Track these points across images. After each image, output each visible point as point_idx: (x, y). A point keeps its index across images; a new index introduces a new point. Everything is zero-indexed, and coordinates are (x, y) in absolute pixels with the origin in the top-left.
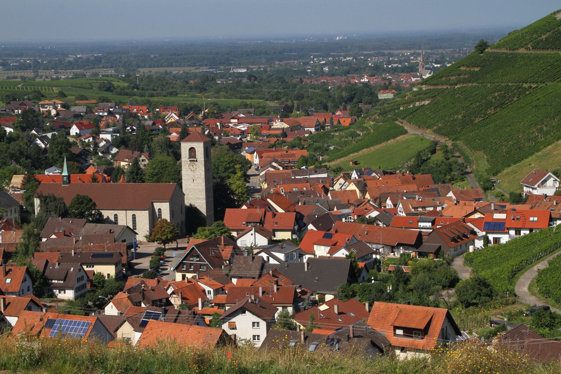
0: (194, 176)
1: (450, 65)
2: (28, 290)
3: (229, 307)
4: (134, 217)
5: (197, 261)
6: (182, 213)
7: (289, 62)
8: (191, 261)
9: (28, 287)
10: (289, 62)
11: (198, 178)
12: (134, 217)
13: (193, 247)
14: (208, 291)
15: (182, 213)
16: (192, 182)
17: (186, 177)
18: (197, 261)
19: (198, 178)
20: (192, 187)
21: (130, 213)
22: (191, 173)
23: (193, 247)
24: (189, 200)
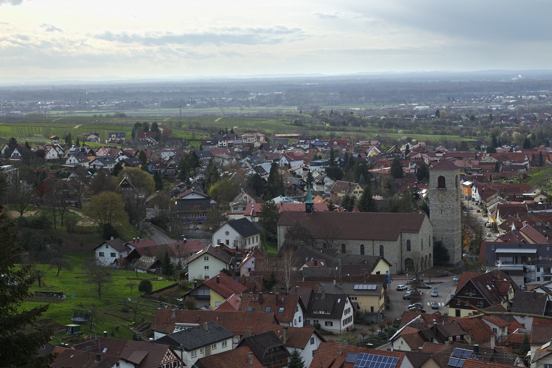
0: (442, 206)
1: (530, 135)
2: (300, 321)
3: (175, 351)
4: (382, 248)
5: (473, 296)
6: (430, 246)
7: (76, 212)
8: (468, 295)
9: (300, 318)
10: (76, 212)
11: (447, 208)
12: (382, 248)
13: (470, 281)
14: (494, 329)
15: (430, 246)
16: (440, 213)
17: (434, 208)
18: (473, 296)
19: (447, 208)
20: (440, 218)
21: (377, 244)
22: (440, 204)
23: (470, 281)
24: (436, 232)
